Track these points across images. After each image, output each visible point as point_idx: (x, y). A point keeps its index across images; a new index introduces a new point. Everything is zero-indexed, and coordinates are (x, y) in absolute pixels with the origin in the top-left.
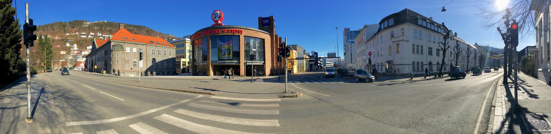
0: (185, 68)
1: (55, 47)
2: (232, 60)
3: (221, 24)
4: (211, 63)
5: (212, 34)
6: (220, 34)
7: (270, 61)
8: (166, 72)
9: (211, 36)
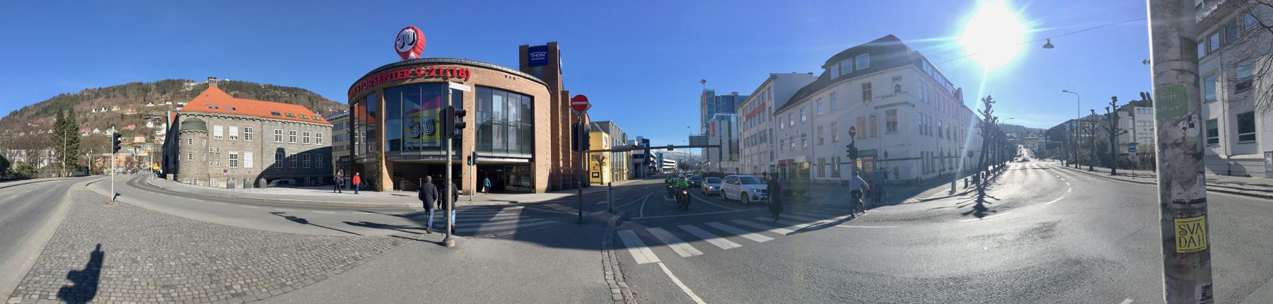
1: (124, 128)
2: (439, 149)
4: (386, 157)
6: (408, 82)
7: (547, 153)
8: (320, 180)
9: (385, 89)
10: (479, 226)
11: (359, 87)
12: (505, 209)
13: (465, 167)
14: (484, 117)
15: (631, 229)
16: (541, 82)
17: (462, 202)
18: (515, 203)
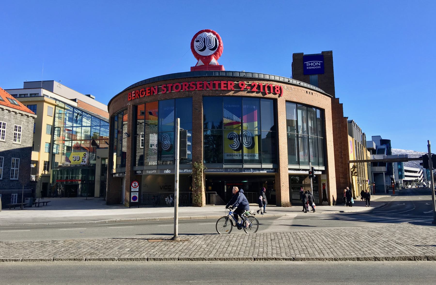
0: (36, 182)
3: (220, 67)
5: (208, 92)
6: (231, 93)
9: (203, 96)
16: (323, 92)
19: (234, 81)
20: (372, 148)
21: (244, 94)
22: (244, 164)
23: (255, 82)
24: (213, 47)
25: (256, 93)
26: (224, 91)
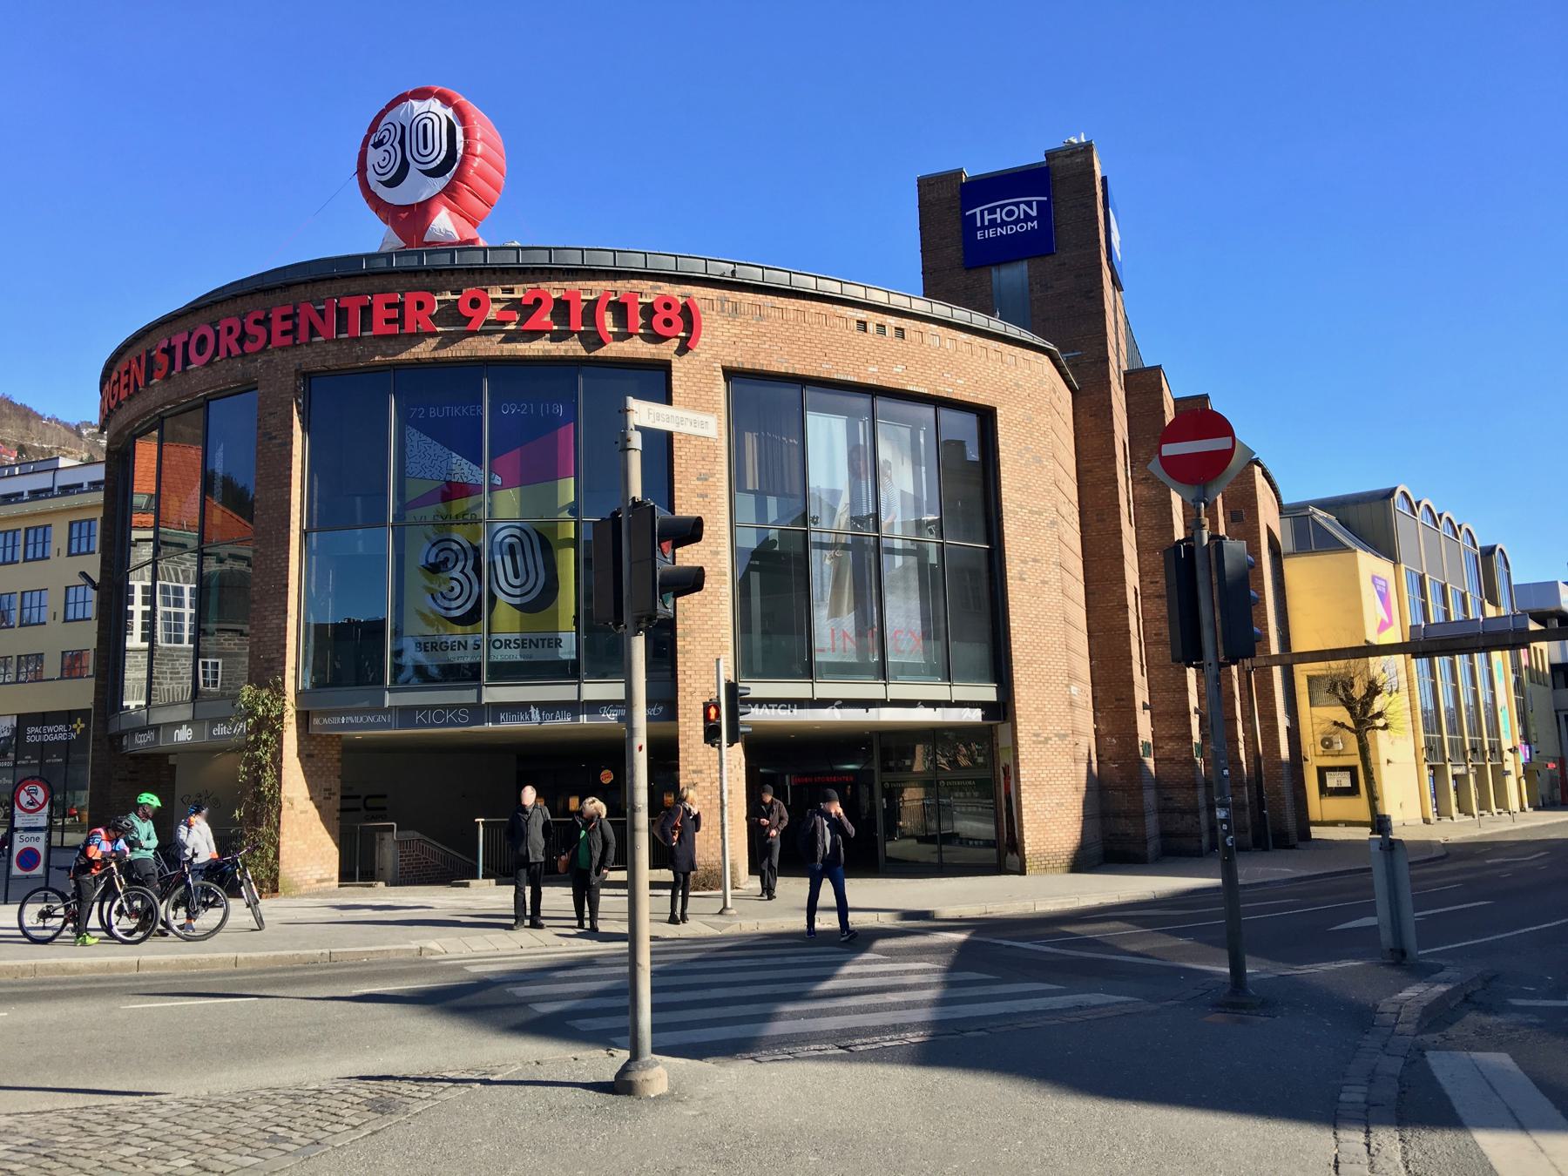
2: (569, 672)
4: (304, 718)
6: (424, 350)
9: (308, 377)
10: (768, 1018)
11: (169, 351)
12: (881, 944)
13: (693, 751)
14: (773, 515)
15: (1499, 1046)
16: (1027, 336)
17: (703, 922)
18: (922, 920)
19: (441, 290)
20: (1553, 608)
21: (491, 347)
22: (585, 683)
23: (543, 286)
24: (438, 162)
25: (552, 340)
26: (392, 343)
